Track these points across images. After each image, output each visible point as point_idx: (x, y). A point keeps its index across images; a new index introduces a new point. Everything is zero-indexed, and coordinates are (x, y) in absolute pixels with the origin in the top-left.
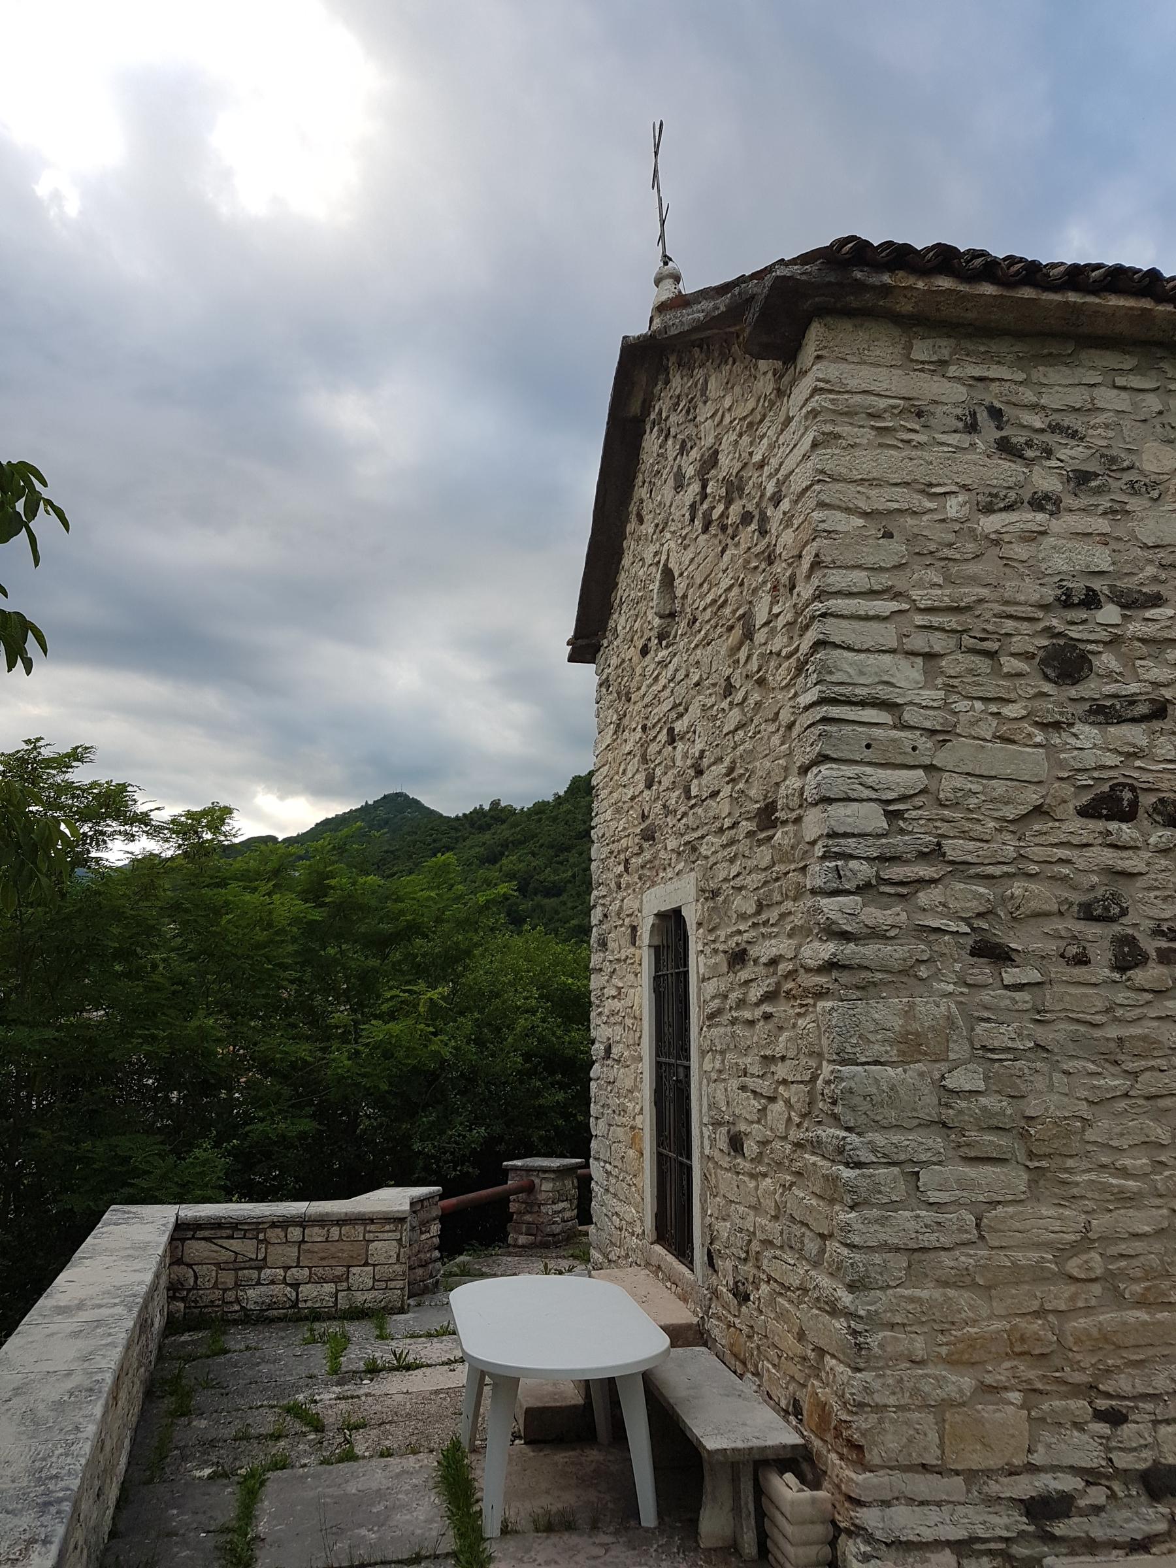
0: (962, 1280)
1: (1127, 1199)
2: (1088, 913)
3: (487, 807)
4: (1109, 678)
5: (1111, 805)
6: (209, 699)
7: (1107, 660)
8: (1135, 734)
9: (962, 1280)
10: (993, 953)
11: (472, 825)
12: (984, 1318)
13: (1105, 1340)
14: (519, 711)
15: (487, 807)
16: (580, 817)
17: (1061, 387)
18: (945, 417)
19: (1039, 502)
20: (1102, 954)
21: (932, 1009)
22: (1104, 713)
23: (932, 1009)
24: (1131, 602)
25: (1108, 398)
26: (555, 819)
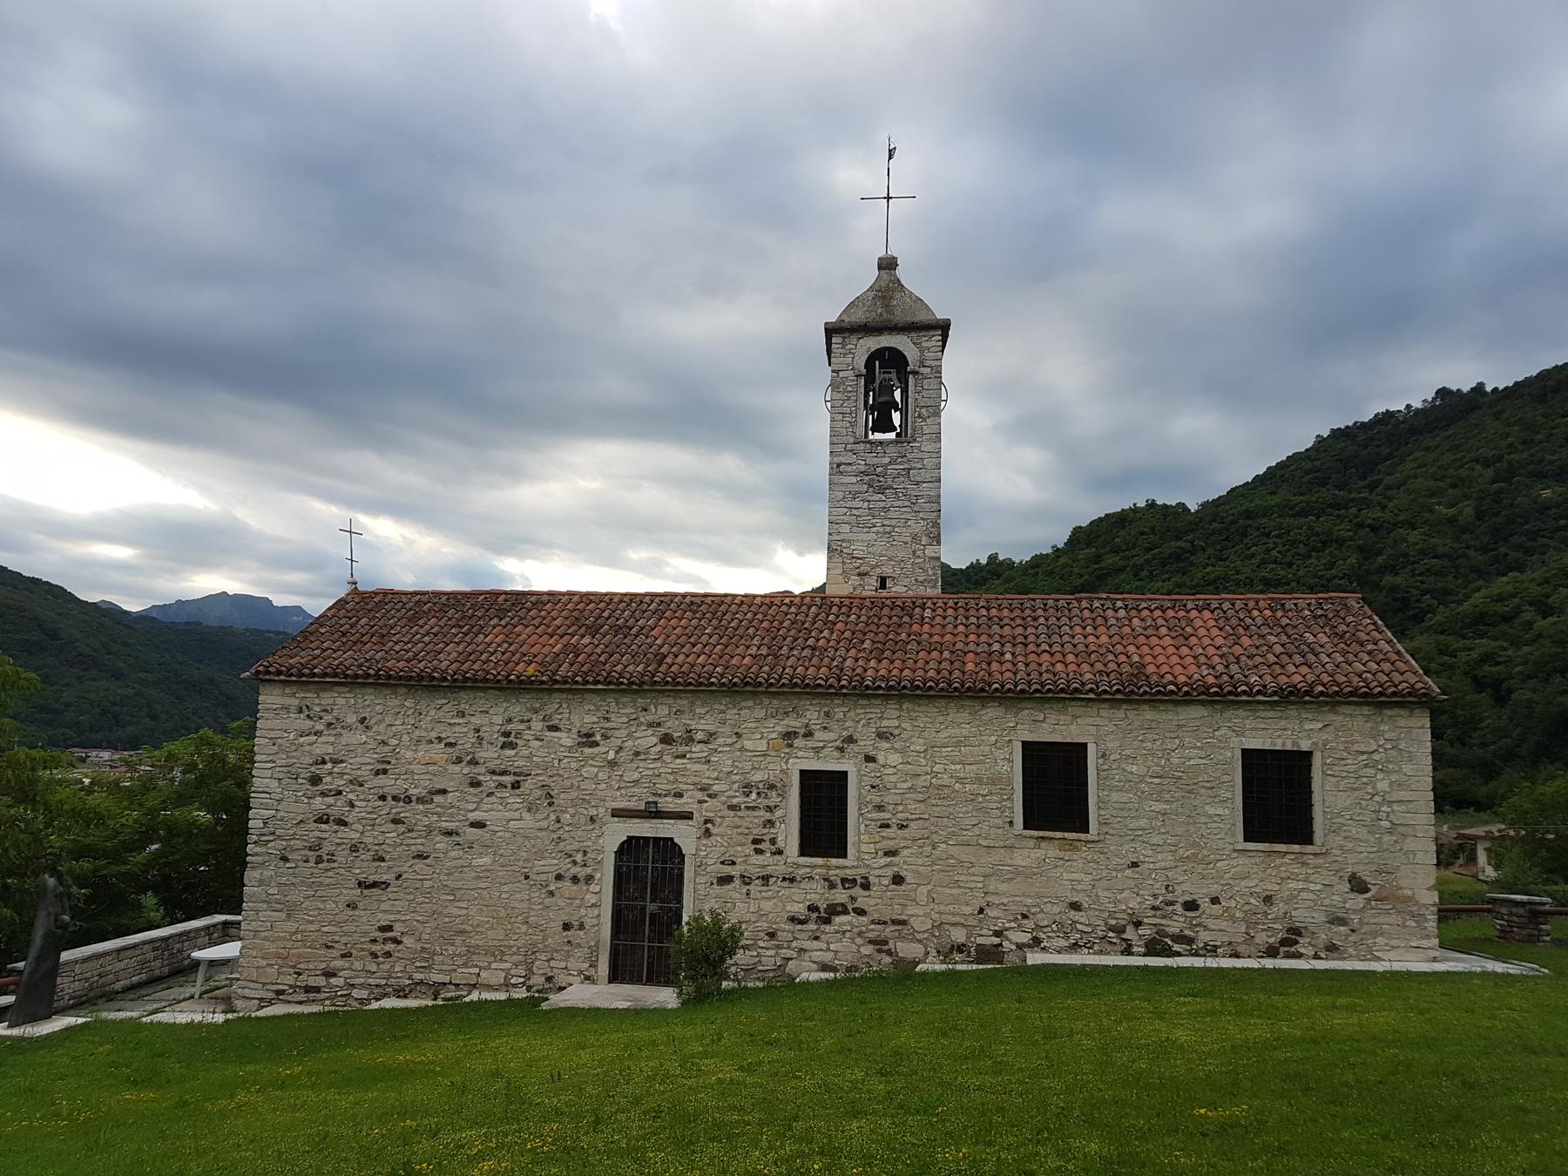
0: (265, 939)
1: (311, 922)
2: (310, 849)
3: (984, 561)
4: (328, 783)
5: (322, 819)
6: (729, 464)
7: (328, 779)
8: (330, 800)
9: (265, 939)
10: (285, 859)
11: (968, 580)
12: (272, 948)
13: (299, 955)
14: (1032, 456)
15: (984, 561)
16: (1076, 570)
17: (327, 698)
18: (293, 709)
19: (318, 733)
20: (313, 860)
21: (267, 873)
22: (323, 794)
23: (267, 873)
24: (335, 762)
25: (341, 701)
26: (1050, 574)
